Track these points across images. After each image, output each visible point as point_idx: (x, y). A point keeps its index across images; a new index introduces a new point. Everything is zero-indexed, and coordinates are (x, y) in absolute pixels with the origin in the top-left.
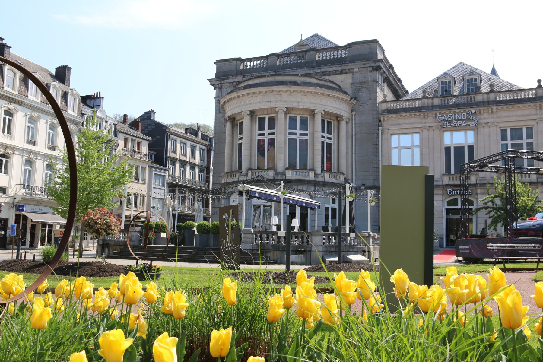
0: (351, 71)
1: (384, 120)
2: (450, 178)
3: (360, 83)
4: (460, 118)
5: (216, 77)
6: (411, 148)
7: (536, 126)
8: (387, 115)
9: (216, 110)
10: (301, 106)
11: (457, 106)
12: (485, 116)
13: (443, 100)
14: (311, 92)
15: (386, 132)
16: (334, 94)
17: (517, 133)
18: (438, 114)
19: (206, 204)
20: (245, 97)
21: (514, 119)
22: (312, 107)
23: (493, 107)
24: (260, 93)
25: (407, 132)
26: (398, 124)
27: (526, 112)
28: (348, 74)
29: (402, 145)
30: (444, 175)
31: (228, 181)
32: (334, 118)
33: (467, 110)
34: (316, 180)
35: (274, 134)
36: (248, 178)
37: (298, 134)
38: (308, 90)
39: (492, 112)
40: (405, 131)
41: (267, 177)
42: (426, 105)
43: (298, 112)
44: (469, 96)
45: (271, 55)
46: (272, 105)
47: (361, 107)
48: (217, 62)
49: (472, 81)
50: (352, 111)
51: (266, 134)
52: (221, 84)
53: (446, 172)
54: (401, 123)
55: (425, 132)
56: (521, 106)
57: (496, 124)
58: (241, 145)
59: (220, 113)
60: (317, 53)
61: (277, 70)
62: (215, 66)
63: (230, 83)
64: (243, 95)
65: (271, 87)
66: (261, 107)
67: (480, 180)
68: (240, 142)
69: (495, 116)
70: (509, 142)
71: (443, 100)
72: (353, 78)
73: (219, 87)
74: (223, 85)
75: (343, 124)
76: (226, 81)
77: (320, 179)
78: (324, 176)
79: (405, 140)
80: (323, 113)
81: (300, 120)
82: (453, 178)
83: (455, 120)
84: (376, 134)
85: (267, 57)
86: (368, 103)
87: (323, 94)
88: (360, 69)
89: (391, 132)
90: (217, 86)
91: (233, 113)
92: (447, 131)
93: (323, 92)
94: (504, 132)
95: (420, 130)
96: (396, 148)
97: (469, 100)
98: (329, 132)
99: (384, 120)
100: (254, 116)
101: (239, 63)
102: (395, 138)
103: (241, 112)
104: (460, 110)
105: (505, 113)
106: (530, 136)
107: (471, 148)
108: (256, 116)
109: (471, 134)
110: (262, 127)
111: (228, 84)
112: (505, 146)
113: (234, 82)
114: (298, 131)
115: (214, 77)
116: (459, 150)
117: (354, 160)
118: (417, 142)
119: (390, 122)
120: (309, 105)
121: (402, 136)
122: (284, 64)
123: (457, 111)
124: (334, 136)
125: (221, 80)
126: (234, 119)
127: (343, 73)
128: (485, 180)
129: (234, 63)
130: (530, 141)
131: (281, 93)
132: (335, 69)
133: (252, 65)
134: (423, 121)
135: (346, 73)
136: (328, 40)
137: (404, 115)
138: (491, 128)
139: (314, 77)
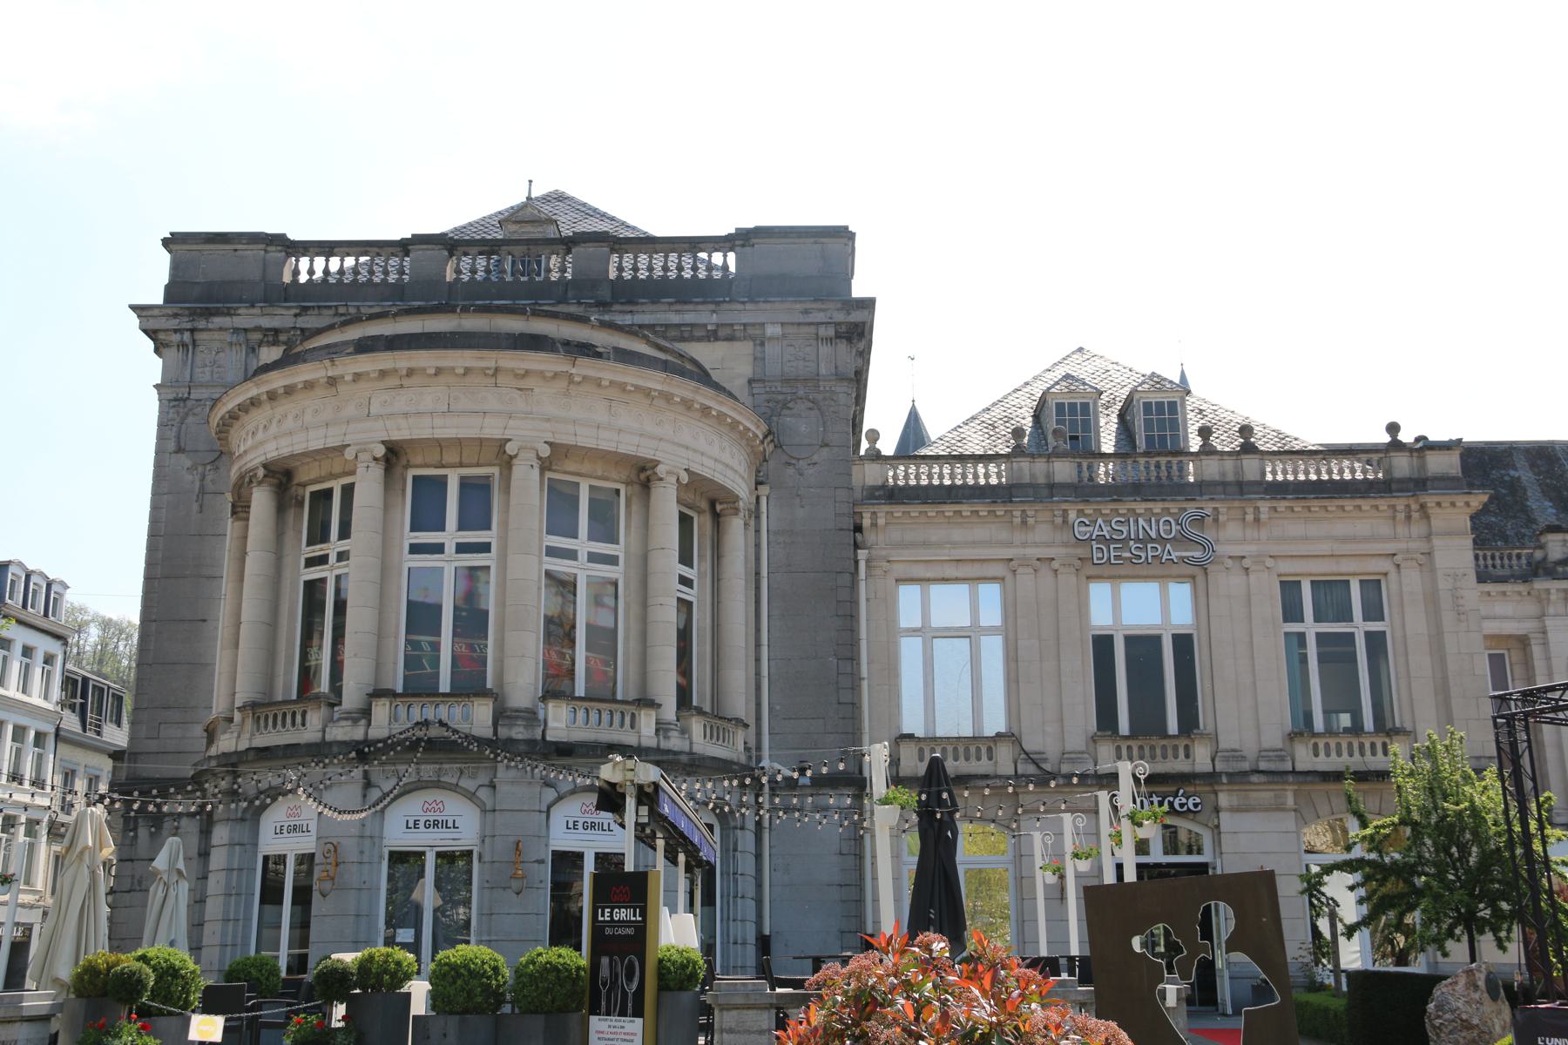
0: (750, 331)
1: (874, 525)
2: (1118, 748)
3: (786, 381)
4: (1153, 534)
5: (166, 300)
6: (971, 634)
7: (1393, 576)
8: (887, 508)
9: (161, 438)
10: (607, 441)
11: (1115, 492)
12: (1232, 535)
13: (1085, 465)
14: (647, 393)
15: (878, 572)
16: (724, 409)
17: (1332, 598)
18: (1072, 515)
19: (1456, 870)
20: (362, 385)
21: (1324, 548)
22: (646, 451)
23: (1260, 504)
24: (439, 371)
25: (959, 574)
26: (926, 544)
27: (1362, 527)
28: (737, 344)
29: (937, 621)
30: (1094, 740)
31: (262, 741)
32: (704, 505)
33: (1174, 507)
34: (664, 745)
35: (552, 552)
36: (374, 733)
37: (583, 556)
38: (641, 383)
39: (1257, 520)
40: (950, 571)
41: (464, 727)
42: (1027, 480)
43: (586, 467)
44: (1153, 461)
45: (419, 240)
46: (492, 429)
47: (790, 471)
48: (166, 243)
49: (1156, 415)
50: (758, 483)
51: (450, 548)
52: (192, 331)
53: (1099, 729)
54: (934, 538)
55: (1025, 578)
56: (1349, 504)
57: (1270, 562)
58: (686, 559)
59: (180, 450)
60: (613, 251)
61: (446, 299)
62: (164, 258)
63: (236, 330)
64: (357, 377)
65: (493, 354)
66: (440, 434)
67: (1226, 759)
68: (314, 573)
69: (1264, 534)
70: (1310, 628)
71: (1085, 465)
72: (758, 360)
73: (184, 345)
74: (198, 336)
75: (736, 528)
76: (218, 321)
77: (675, 742)
78: (684, 731)
79: (950, 604)
80: (685, 478)
81: (591, 501)
82: (1129, 748)
83: (1138, 540)
84: (847, 577)
85: (404, 247)
86: (815, 458)
87: (687, 404)
88: (790, 330)
89: (899, 570)
90: (176, 338)
91: (285, 451)
92: (1099, 578)
93: (689, 395)
94: (1290, 589)
95: (1007, 572)
96: (914, 632)
97: (1164, 474)
98: (313, 590)
99: (874, 525)
100: (398, 470)
101: (275, 254)
102: (908, 597)
103: (341, 449)
104: (1150, 505)
105: (1294, 528)
106: (1373, 611)
107: (1183, 643)
108: (407, 467)
109: (1181, 594)
110: (427, 515)
111: (228, 337)
112: (1295, 641)
113: (257, 329)
114: (583, 544)
115: (158, 299)
116: (1143, 647)
117: (765, 672)
118: (992, 615)
119: (895, 535)
120: (636, 440)
121: (935, 589)
122: (472, 279)
123: (1140, 507)
124: (701, 575)
125: (194, 314)
126: (288, 474)
127: (717, 339)
128: (1244, 758)
129: (257, 251)
130: (1295, 627)
131: (529, 382)
132: (689, 318)
133: (319, 274)
134: (1018, 537)
135: (730, 338)
136: (613, 219)
137: (949, 509)
138: (1252, 577)
139: (645, 337)
